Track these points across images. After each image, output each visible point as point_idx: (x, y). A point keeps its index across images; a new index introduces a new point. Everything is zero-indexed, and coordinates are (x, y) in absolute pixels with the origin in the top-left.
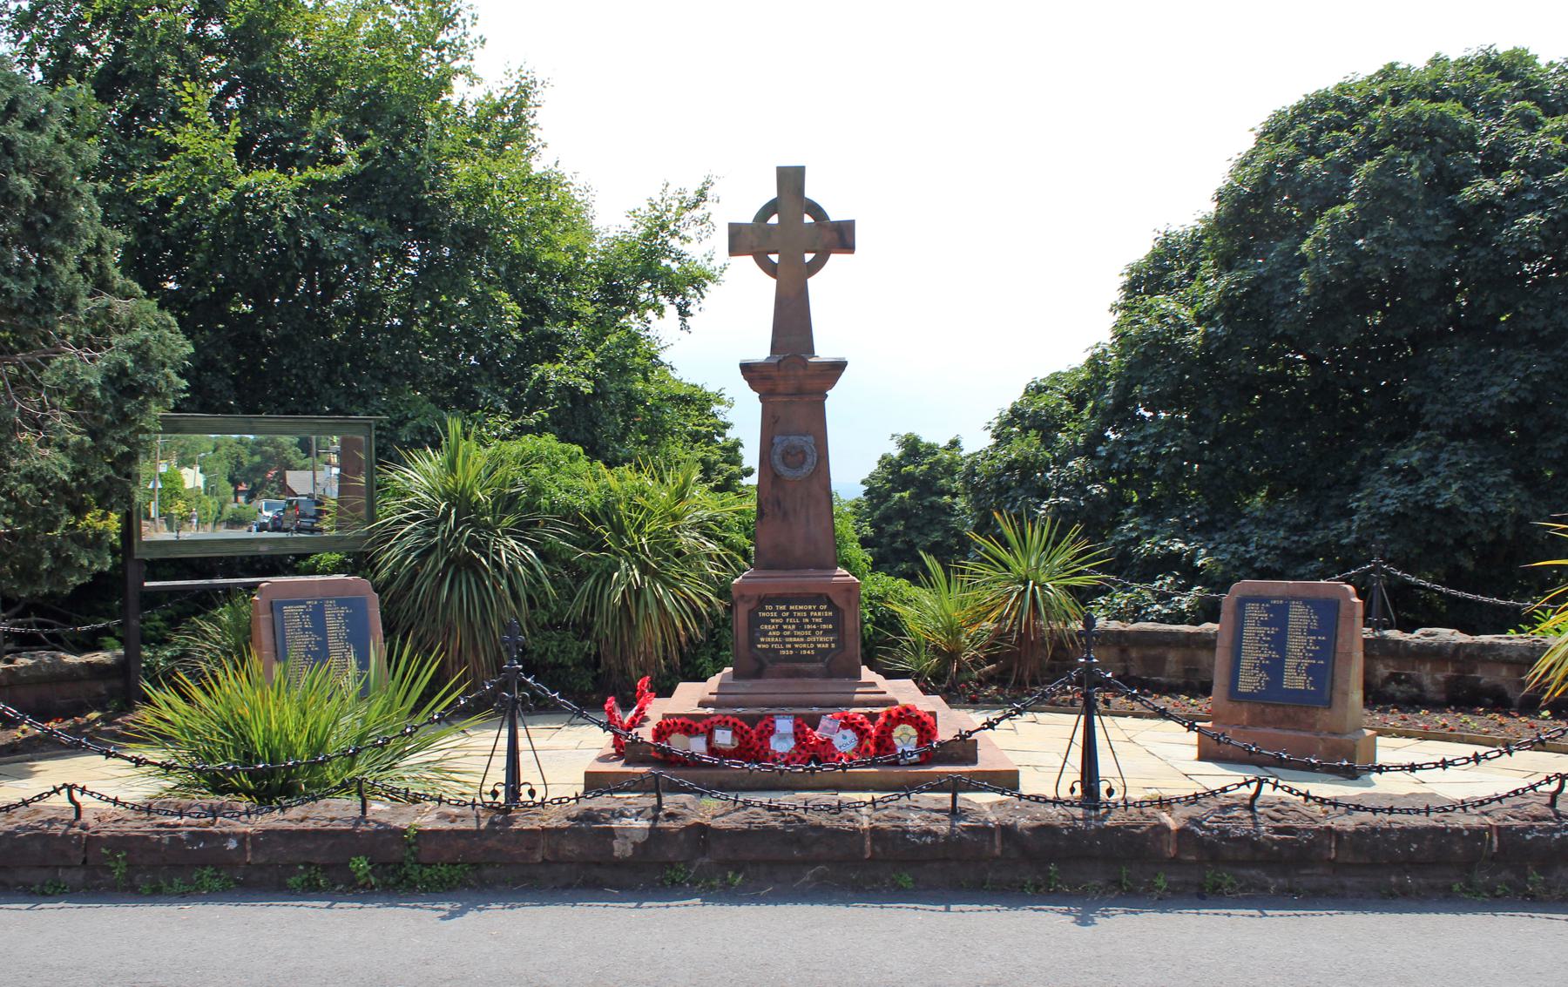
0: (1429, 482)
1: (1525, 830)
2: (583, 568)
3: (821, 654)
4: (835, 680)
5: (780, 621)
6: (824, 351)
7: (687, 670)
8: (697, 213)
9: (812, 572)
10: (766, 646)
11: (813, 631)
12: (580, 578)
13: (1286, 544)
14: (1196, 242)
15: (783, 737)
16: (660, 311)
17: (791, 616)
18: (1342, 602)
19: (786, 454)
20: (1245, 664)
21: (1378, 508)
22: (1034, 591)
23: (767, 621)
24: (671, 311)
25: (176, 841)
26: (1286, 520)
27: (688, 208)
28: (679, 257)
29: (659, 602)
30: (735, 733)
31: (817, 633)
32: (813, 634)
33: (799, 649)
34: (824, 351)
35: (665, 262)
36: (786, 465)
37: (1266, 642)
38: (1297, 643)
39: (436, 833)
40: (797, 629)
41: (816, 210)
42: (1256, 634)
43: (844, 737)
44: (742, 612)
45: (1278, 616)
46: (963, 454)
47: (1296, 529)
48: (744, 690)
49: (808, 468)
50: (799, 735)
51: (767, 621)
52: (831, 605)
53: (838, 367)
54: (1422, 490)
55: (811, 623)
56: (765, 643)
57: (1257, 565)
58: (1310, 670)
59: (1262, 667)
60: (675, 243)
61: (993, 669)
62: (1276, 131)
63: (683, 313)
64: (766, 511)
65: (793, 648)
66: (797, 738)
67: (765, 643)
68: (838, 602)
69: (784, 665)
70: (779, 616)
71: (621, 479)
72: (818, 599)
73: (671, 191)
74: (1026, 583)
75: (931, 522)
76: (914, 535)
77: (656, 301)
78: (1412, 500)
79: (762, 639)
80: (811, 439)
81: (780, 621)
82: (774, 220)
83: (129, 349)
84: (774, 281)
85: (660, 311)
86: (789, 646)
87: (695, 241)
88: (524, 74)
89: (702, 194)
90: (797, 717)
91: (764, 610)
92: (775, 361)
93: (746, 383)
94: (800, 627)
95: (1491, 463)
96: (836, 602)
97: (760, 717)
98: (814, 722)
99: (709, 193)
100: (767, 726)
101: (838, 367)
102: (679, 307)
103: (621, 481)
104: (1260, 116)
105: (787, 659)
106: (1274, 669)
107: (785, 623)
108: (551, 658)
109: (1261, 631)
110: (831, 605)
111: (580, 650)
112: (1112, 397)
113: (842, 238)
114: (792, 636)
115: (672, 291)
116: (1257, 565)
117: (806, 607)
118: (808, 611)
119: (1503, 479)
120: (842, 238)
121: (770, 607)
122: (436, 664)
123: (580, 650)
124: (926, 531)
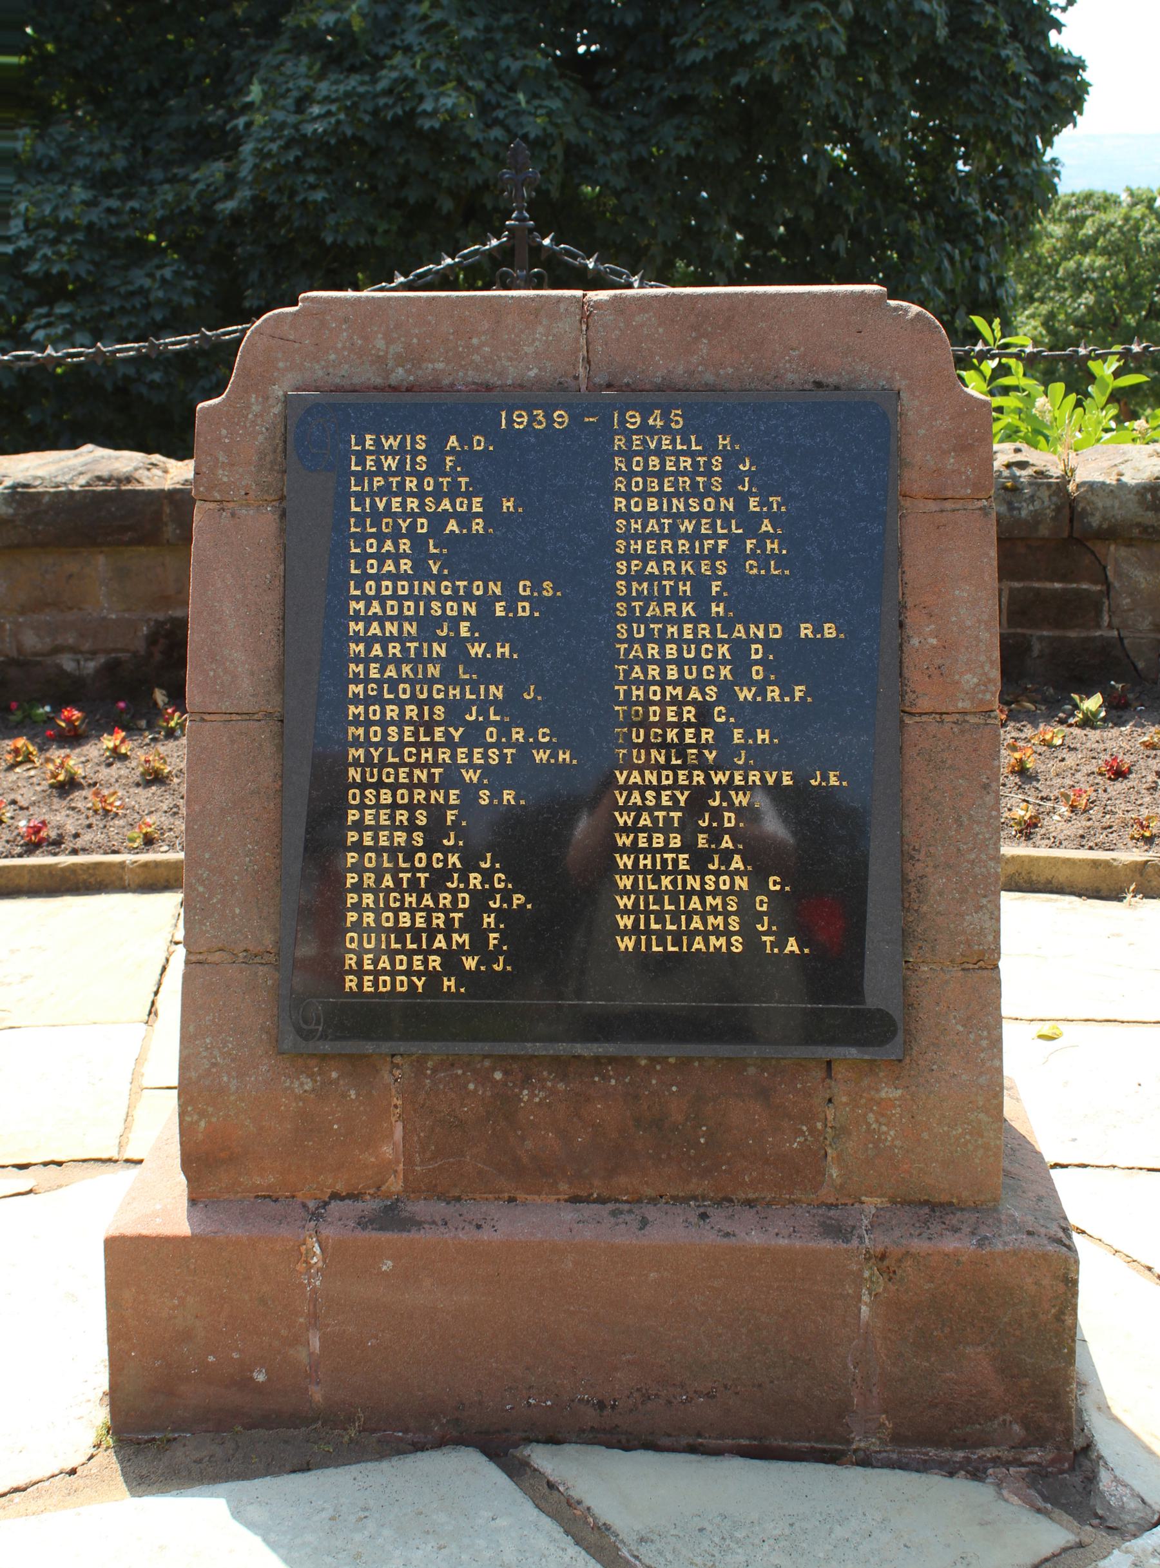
0: (399, 66)
13: (94, 215)
18: (912, 406)
21: (296, 127)
26: (82, 162)
37: (487, 670)
42: (428, 626)
47: (103, 183)
54: (382, 85)
57: (33, 267)
61: (19, 67)
78: (370, 107)
95: (506, 29)
116: (33, 267)
119: (542, 62)
122: (230, 329)
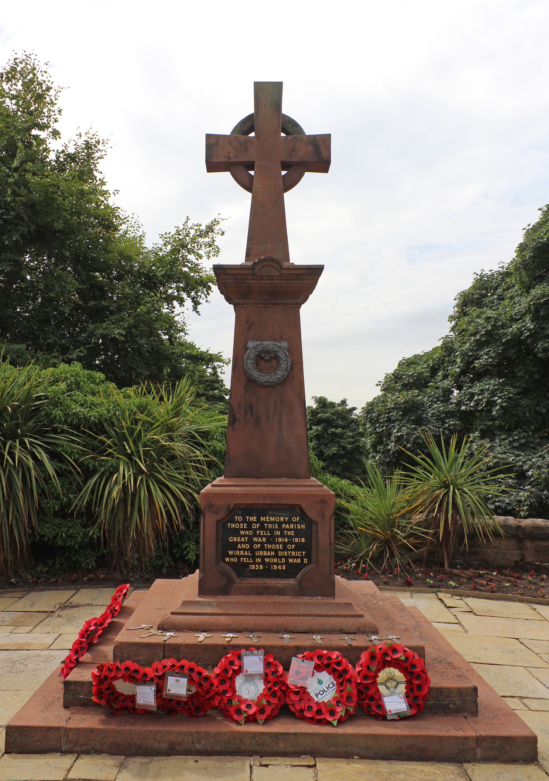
4: (307, 599)
5: (251, 533)
7: (175, 551)
9: (284, 481)
10: (235, 560)
11: (285, 544)
12: (88, 473)
14: (506, 274)
15: (250, 677)
16: (181, 302)
17: (262, 528)
19: (259, 358)
22: (454, 492)
24: (189, 303)
27: (201, 236)
30: (191, 681)
31: (289, 547)
32: (285, 549)
33: (269, 564)
36: (260, 370)
40: (268, 542)
43: (320, 682)
46: (347, 408)
48: (209, 610)
49: (280, 373)
50: (271, 678)
51: (236, 533)
52: (304, 517)
53: (317, 271)
55: (282, 535)
56: (233, 556)
60: (191, 257)
63: (196, 303)
64: (238, 416)
65: (263, 563)
66: (266, 678)
67: (233, 556)
68: (312, 514)
69: (254, 581)
70: (249, 528)
73: (190, 224)
74: (447, 487)
75: (332, 441)
76: (323, 448)
77: (179, 294)
79: (231, 553)
80: (285, 344)
81: (251, 533)
84: (250, 195)
85: (181, 302)
86: (259, 560)
87: (205, 258)
88: (90, 136)
89: (210, 229)
90: (268, 651)
91: (233, 521)
92: (250, 263)
93: (222, 297)
96: (309, 514)
97: (226, 648)
99: (216, 228)
100: (232, 663)
101: (317, 271)
107: (255, 535)
108: (60, 542)
111: (85, 535)
112: (459, 367)
114: (262, 549)
115: (187, 289)
117: (277, 519)
118: (280, 524)
121: (240, 518)
123: (85, 535)
124: (329, 446)
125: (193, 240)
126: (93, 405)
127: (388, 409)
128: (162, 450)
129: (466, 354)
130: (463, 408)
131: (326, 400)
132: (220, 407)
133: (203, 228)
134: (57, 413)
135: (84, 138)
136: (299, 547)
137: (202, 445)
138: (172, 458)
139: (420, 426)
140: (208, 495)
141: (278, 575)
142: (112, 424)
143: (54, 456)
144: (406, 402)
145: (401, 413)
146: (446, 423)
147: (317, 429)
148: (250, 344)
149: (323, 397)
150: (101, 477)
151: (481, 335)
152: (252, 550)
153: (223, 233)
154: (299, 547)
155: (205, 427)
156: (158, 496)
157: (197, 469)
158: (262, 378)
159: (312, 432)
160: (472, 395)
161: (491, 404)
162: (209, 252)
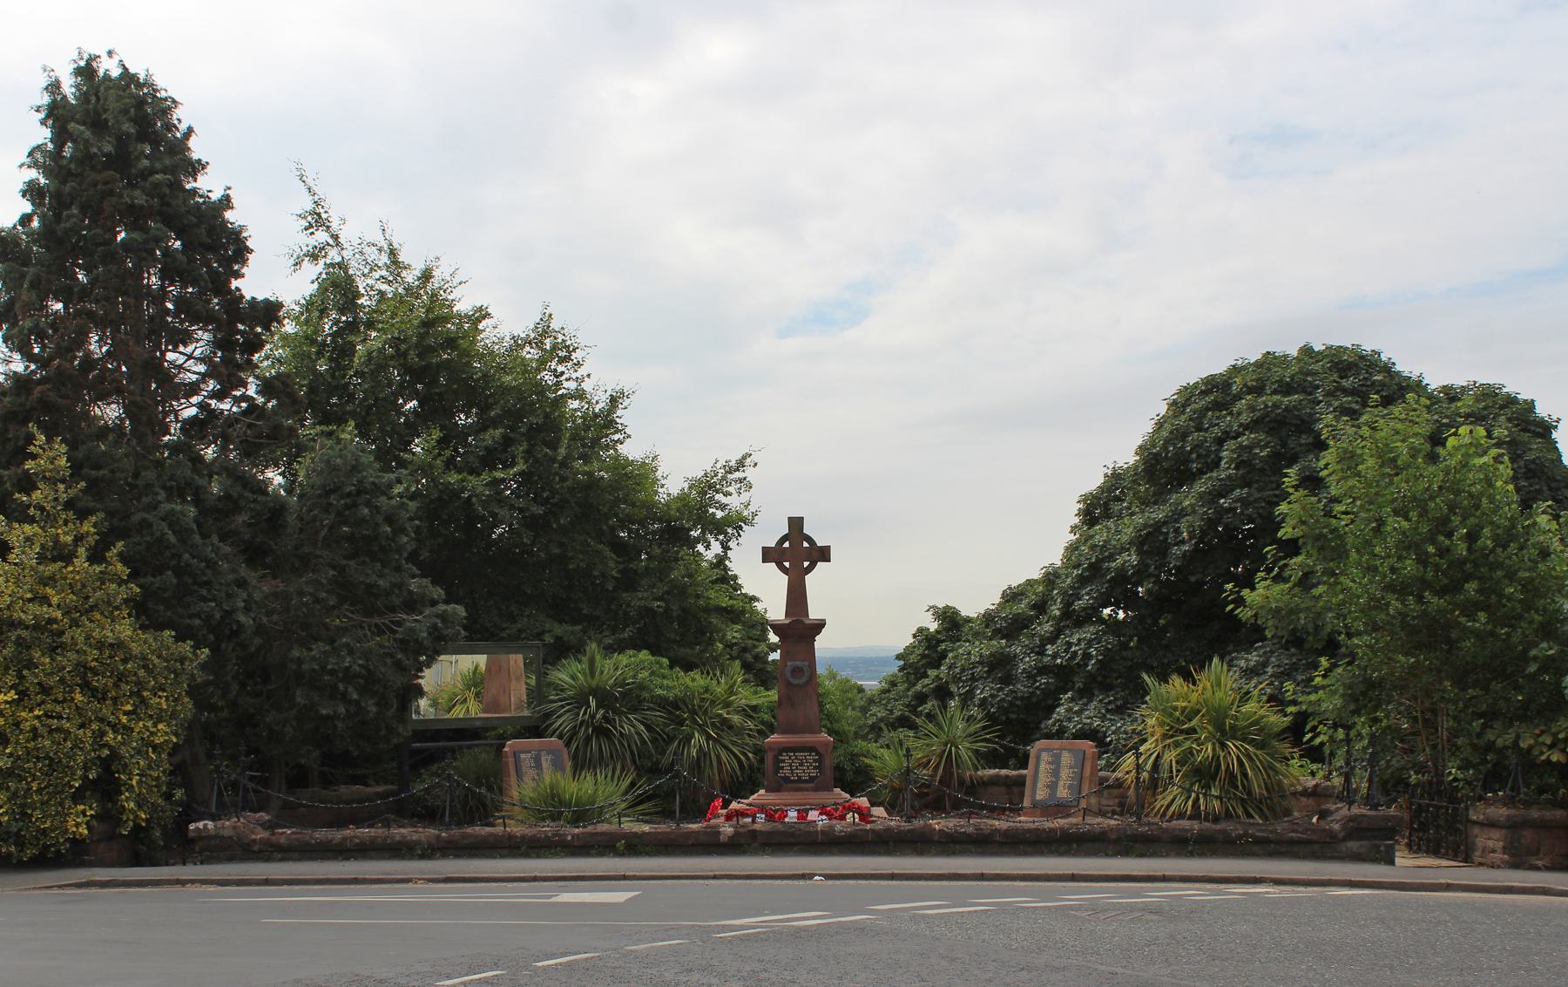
1: (1069, 829)
2: (671, 735)
3: (812, 779)
6: (814, 614)
8: (737, 475)
9: (808, 735)
12: (671, 739)
20: (1040, 785)
23: (783, 761)
25: (547, 837)
28: (723, 507)
29: (718, 757)
34: (814, 614)
35: (711, 511)
38: (1065, 773)
39: (650, 833)
41: (810, 540)
44: (769, 758)
45: (1056, 761)
49: (804, 679)
51: (783, 761)
58: (1070, 787)
59: (1048, 786)
60: (719, 497)
62: (1179, 404)
68: (821, 750)
69: (792, 785)
71: (693, 680)
72: (810, 749)
80: (807, 663)
82: (787, 545)
83: (437, 616)
89: (741, 464)
90: (798, 811)
92: (787, 622)
94: (801, 764)
98: (807, 811)
102: (722, 544)
103: (696, 680)
104: (1171, 390)
105: (795, 781)
106: (1053, 787)
109: (1047, 766)
110: (818, 753)
113: (824, 554)
120: (824, 554)
125: (724, 478)
126: (668, 688)
127: (972, 663)
128: (725, 721)
129: (1066, 592)
130: (1059, 661)
131: (956, 613)
132: (735, 634)
133: (733, 463)
134: (645, 695)
135: (608, 393)
136: (815, 768)
137: (751, 717)
138: (730, 727)
139: (1008, 685)
140: (768, 742)
141: (806, 781)
142: (684, 702)
143: (649, 728)
144: (992, 655)
145: (986, 669)
146: (1037, 681)
147: (937, 676)
148: (789, 664)
149: (951, 608)
150: (679, 743)
151: (1083, 569)
152: (791, 770)
153: (756, 464)
154: (815, 768)
155: (754, 703)
156: (724, 755)
157: (749, 735)
158: (795, 681)
159: (926, 681)
160: (1069, 645)
161: (1087, 656)
162: (740, 489)
